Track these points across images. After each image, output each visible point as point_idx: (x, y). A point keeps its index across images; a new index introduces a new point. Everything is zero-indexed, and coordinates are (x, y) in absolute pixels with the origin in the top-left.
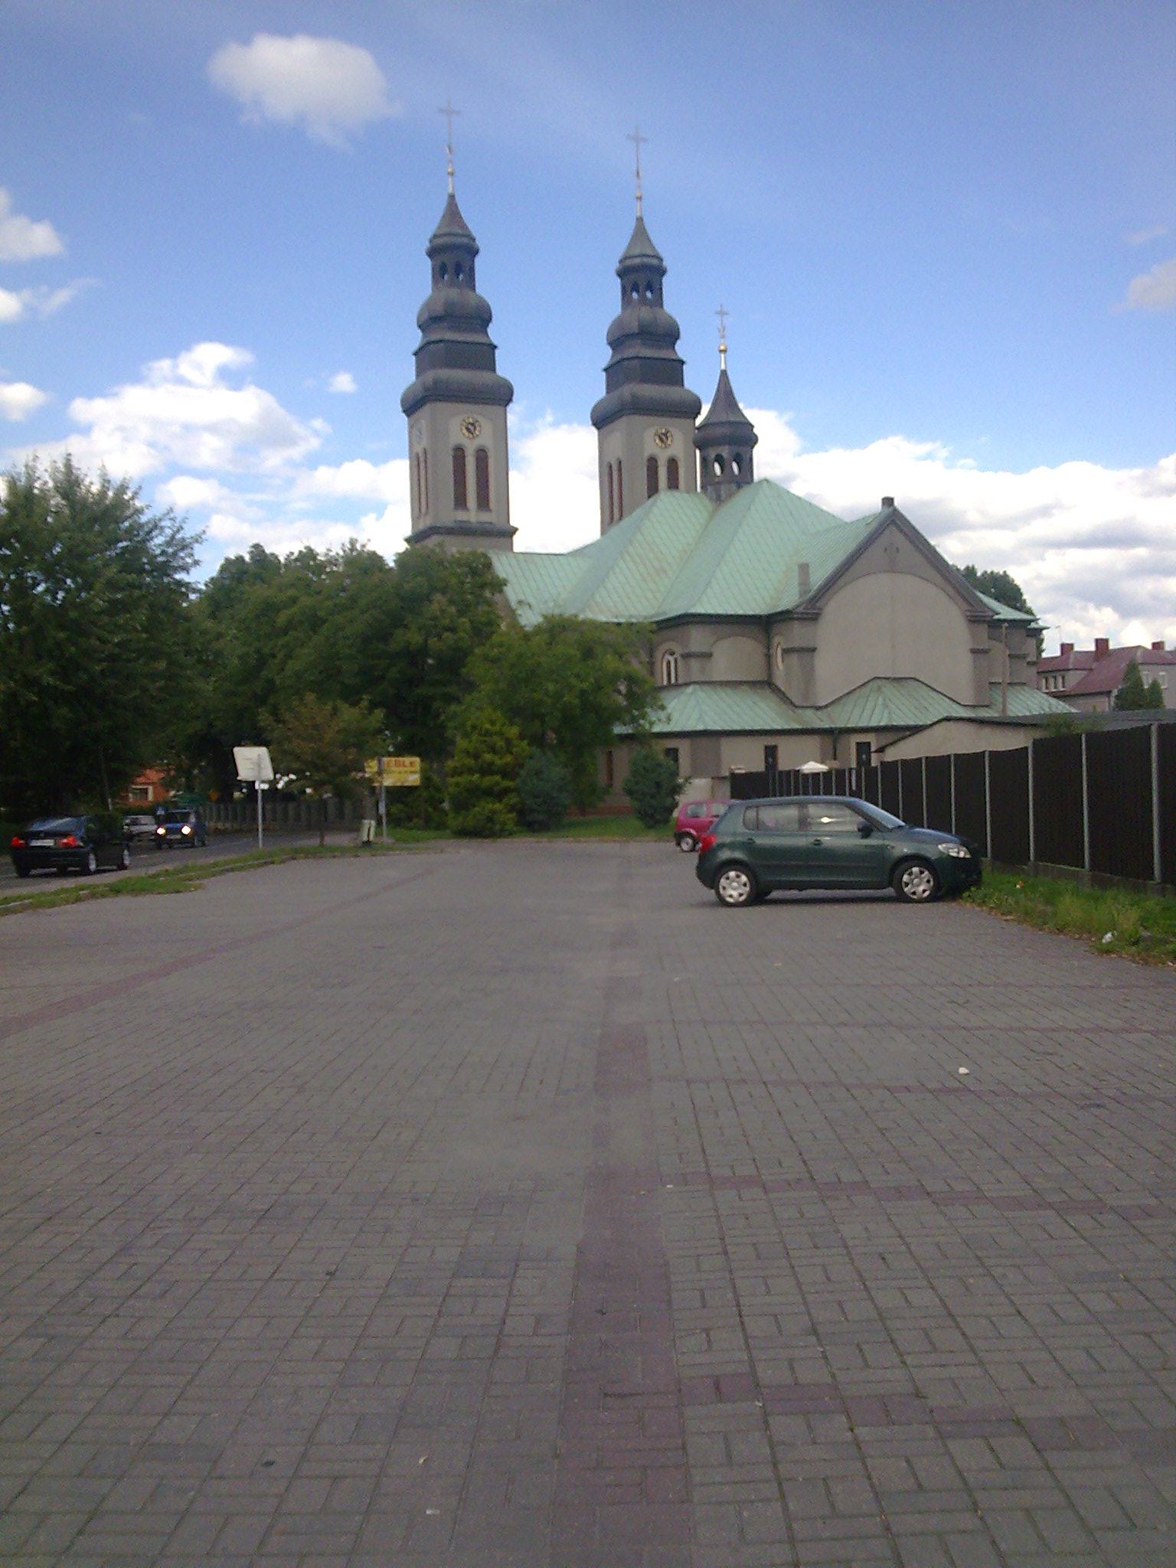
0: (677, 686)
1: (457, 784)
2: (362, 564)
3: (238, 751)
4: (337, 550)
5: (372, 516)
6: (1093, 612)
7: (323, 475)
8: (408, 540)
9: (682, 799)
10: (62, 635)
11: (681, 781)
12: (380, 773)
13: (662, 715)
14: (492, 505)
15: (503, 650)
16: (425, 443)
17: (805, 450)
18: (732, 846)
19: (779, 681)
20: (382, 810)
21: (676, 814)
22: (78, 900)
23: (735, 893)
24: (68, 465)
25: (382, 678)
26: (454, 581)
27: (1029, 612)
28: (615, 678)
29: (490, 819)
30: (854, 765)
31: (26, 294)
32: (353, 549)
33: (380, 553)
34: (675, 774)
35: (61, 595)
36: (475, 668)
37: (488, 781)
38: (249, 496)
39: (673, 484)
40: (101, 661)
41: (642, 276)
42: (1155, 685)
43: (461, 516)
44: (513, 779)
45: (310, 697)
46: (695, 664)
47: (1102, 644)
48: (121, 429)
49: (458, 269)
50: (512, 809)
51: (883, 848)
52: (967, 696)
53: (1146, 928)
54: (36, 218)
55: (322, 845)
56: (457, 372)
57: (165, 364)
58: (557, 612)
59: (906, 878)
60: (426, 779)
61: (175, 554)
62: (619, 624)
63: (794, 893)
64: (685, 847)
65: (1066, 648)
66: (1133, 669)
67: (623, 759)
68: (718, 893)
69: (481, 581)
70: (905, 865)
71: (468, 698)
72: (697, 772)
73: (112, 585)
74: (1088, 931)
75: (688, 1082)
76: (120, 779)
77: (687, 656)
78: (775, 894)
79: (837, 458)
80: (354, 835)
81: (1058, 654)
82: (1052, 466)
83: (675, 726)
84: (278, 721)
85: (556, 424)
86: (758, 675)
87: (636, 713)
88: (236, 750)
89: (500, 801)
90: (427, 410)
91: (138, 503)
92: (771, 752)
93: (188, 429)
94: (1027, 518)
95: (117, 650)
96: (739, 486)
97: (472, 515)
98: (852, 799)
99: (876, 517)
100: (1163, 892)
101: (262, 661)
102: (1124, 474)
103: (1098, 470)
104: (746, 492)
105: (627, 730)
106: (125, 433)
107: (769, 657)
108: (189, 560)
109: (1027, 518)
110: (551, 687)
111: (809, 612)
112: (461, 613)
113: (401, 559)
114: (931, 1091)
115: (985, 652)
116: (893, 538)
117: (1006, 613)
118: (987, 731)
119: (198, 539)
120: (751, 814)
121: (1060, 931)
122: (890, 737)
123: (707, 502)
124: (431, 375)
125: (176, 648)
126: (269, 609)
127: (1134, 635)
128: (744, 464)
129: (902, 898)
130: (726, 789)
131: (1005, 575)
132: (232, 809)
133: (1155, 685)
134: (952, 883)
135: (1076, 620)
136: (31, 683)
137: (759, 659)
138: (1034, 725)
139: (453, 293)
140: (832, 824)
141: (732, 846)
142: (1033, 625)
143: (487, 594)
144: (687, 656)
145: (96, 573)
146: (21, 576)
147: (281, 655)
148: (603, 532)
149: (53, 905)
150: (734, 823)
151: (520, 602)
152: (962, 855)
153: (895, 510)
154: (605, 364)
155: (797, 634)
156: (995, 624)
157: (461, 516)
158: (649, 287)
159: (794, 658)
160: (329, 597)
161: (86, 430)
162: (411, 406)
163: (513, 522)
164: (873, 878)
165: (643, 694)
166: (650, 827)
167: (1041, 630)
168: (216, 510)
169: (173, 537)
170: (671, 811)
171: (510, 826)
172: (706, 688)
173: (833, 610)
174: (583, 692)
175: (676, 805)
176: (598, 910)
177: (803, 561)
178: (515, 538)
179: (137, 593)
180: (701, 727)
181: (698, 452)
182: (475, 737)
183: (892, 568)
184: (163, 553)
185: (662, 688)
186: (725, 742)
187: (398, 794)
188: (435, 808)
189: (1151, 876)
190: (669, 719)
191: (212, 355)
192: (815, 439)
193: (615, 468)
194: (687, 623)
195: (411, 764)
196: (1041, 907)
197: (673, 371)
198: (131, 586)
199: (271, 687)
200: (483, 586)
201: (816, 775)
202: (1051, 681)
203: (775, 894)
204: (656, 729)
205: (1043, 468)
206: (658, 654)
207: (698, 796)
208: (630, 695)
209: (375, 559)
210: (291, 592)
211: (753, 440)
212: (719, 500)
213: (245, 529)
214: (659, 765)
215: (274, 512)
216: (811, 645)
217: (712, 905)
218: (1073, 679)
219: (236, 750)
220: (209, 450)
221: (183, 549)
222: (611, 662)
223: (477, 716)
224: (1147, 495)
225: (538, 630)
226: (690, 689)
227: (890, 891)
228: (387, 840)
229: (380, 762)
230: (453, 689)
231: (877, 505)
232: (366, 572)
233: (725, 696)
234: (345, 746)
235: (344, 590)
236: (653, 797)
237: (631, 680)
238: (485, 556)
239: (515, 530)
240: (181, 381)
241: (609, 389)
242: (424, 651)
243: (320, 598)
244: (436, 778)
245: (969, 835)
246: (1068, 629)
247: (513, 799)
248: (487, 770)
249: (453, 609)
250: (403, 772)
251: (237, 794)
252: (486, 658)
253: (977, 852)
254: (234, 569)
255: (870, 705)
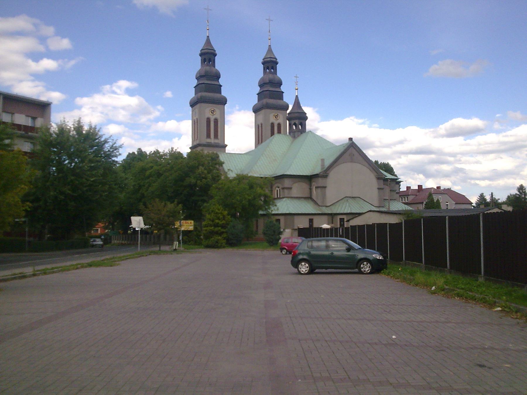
0: (280, 198)
1: (206, 230)
2: (176, 156)
3: (133, 218)
4: (167, 151)
5: (177, 139)
6: (416, 176)
7: (160, 124)
8: (190, 148)
9: (282, 237)
10: (73, 178)
11: (282, 230)
12: (181, 226)
13: (276, 208)
14: (219, 137)
15: (223, 185)
16: (197, 117)
17: (322, 120)
18: (303, 254)
19: (314, 197)
20: (181, 238)
21: (280, 241)
22: (77, 268)
23: (304, 270)
24: (79, 122)
25: (181, 194)
26: (206, 162)
27: (396, 176)
28: (260, 196)
29: (217, 242)
30: (339, 226)
31: (60, 61)
32: (172, 151)
33: (181, 152)
34: (280, 228)
35: (73, 164)
36: (213, 192)
37: (216, 229)
38: (135, 131)
39: (279, 132)
40: (86, 186)
41: (270, 64)
42: (438, 200)
43: (209, 140)
44: (225, 229)
45: (157, 200)
46: (286, 191)
47: (420, 187)
48: (92, 108)
49: (210, 60)
50: (224, 238)
51: (355, 255)
52: (376, 203)
53: (447, 285)
54: (64, 37)
55: (160, 250)
56: (209, 93)
57: (108, 87)
58: (241, 173)
59: (362, 266)
60: (195, 228)
61: (113, 151)
62: (262, 178)
63: (324, 270)
64: (284, 253)
65: (408, 188)
66: (430, 195)
67: (261, 223)
68: (298, 270)
69: (215, 162)
70: (362, 261)
71: (210, 201)
72: (286, 227)
73: (91, 161)
74: (427, 286)
75: (299, 340)
76: (90, 226)
77: (283, 188)
78: (317, 271)
79: (333, 123)
80: (171, 246)
81: (406, 190)
82: (403, 128)
83: (280, 212)
84: (146, 208)
85: (240, 110)
86: (307, 195)
87: (267, 207)
88: (132, 218)
89: (221, 236)
90: (198, 106)
91: (100, 133)
92: (311, 221)
93: (115, 108)
94: (395, 144)
95: (92, 183)
96: (302, 133)
97: (212, 140)
98: (345, 239)
99: (346, 144)
100: (450, 273)
101: (140, 187)
102: (427, 130)
103: (418, 128)
104: (304, 135)
105: (264, 213)
106: (93, 109)
107: (311, 189)
108: (117, 153)
109: (395, 144)
110: (238, 198)
111: (324, 175)
112: (209, 173)
113: (189, 154)
114: (384, 345)
115: (382, 189)
116: (352, 151)
117: (389, 176)
118: (383, 215)
119: (121, 146)
120: (310, 244)
121: (417, 285)
122: (351, 217)
123: (291, 138)
124: (200, 94)
125: (112, 183)
126: (143, 170)
127: (430, 184)
128: (303, 126)
129: (361, 273)
130: (296, 233)
131: (388, 164)
132: (131, 237)
133: (438, 200)
134: (378, 268)
135: (411, 178)
136: (62, 193)
137: (307, 190)
138: (400, 214)
139: (208, 68)
140: (337, 247)
141: (303, 254)
142: (398, 180)
143: (217, 166)
144: (283, 188)
145: (86, 157)
146: (60, 158)
147: (147, 186)
148: (256, 147)
149: (69, 270)
150: (304, 246)
151: (229, 170)
152: (381, 258)
153: (353, 142)
154: (257, 93)
155: (320, 182)
156: (386, 180)
157: (209, 140)
158: (272, 68)
159: (319, 190)
160: (164, 167)
161: (80, 108)
162: (193, 104)
163: (226, 143)
164: (349, 266)
165: (269, 201)
166: (272, 246)
167: (400, 182)
168: (123, 136)
169: (112, 146)
170: (278, 240)
171: (224, 244)
172: (290, 199)
173: (332, 174)
174: (249, 200)
175: (280, 238)
176: (256, 274)
177: (323, 158)
178: (226, 148)
179: (99, 164)
180: (288, 212)
181: (288, 122)
182: (213, 214)
183: (352, 161)
184: (109, 151)
185: (275, 199)
186: (296, 217)
187: (186, 233)
188: (198, 238)
189: (446, 267)
190: (278, 209)
191: (124, 84)
192: (325, 117)
193: (260, 126)
194: (283, 178)
195: (191, 223)
196: (409, 277)
197: (280, 95)
198: (98, 161)
199: (143, 196)
200: (216, 164)
201: (327, 229)
202: (403, 199)
203: (317, 271)
204: (273, 213)
205: (401, 129)
206: (274, 188)
207: (287, 235)
208: (265, 202)
209: (180, 154)
210: (151, 165)
211: (306, 118)
212: (294, 137)
213: (133, 142)
214: (275, 225)
215: (144, 137)
216: (325, 186)
217: (296, 274)
218: (411, 198)
219: (132, 218)
220: (122, 116)
221: (116, 149)
222: (259, 190)
223: (213, 208)
224: (435, 137)
225: (235, 179)
226: (284, 199)
227: (357, 270)
228: (182, 248)
229: (180, 222)
230: (205, 198)
231: (347, 141)
232: (177, 158)
233: (296, 202)
234: (169, 217)
235: (169, 164)
236: (273, 235)
237: (266, 196)
238: (217, 154)
239: (226, 146)
240: (114, 92)
241: (259, 100)
242: (195, 185)
243: (160, 167)
244: (199, 228)
245: (382, 250)
246: (409, 182)
247: (225, 235)
248: (216, 225)
249: (206, 172)
250: (188, 225)
251: (129, 232)
252: (217, 188)
253: (385, 257)
254: (131, 156)
255: (344, 206)
